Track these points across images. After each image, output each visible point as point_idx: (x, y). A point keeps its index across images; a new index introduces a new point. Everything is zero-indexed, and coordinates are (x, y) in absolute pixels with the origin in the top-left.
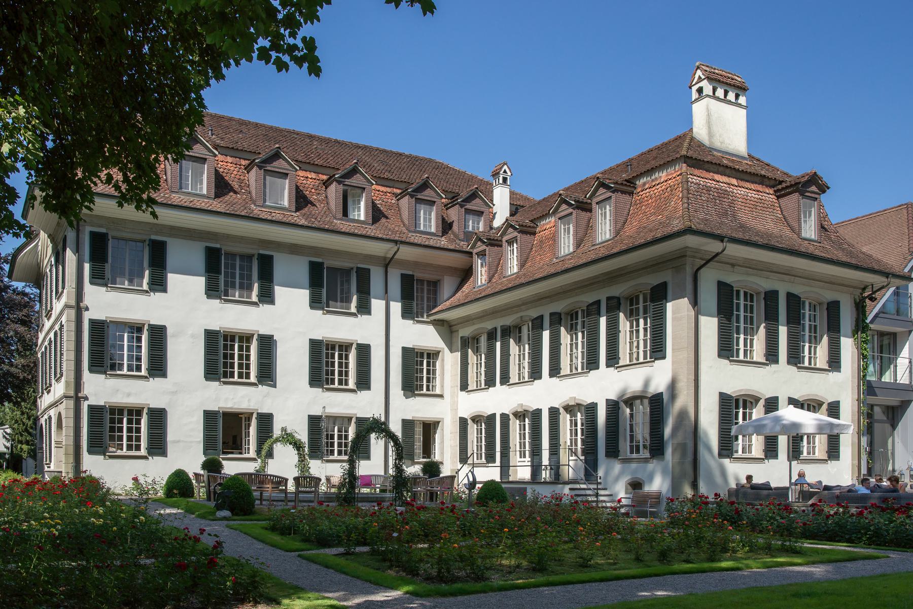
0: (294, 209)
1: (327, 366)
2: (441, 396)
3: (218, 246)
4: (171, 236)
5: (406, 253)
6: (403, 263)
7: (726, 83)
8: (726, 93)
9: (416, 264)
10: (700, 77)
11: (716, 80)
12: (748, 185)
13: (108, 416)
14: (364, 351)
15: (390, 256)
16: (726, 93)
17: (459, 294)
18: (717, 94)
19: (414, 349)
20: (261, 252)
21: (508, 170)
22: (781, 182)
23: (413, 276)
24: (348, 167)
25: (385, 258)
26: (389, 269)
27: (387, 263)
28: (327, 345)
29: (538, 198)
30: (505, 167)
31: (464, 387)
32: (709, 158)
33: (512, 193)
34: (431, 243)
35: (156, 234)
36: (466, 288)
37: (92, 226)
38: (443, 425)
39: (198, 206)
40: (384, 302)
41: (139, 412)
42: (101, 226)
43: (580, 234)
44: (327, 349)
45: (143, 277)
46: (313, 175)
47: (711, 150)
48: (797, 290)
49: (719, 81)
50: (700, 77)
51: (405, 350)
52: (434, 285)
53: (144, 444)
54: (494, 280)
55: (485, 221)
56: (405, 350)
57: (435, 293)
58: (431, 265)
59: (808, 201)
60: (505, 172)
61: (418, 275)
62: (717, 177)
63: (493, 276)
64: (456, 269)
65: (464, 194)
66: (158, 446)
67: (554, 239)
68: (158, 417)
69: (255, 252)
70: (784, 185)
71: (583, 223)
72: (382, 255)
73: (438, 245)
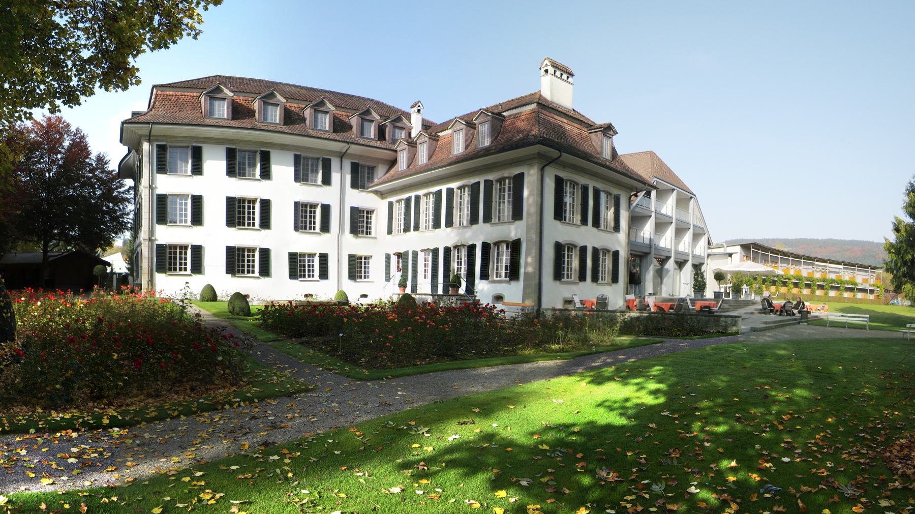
0: (282, 123)
1: (302, 217)
2: (375, 238)
3: (234, 147)
4: (204, 143)
5: (354, 149)
6: (352, 156)
7: (562, 70)
8: (562, 75)
9: (361, 156)
10: (546, 64)
11: (556, 67)
12: (573, 124)
13: (168, 250)
14: (326, 209)
15: (344, 151)
16: (562, 75)
17: (388, 175)
18: (556, 74)
19: (358, 208)
20: (262, 149)
21: (421, 106)
22: (591, 126)
23: (358, 164)
24: (318, 100)
25: (340, 152)
26: (343, 159)
27: (342, 156)
28: (302, 205)
29: (439, 123)
30: (419, 104)
31: (390, 232)
32: (551, 106)
33: (423, 120)
34: (371, 144)
35: (196, 142)
36: (392, 172)
37: (158, 141)
38: (377, 213)
39: (221, 124)
40: (340, 175)
41: (186, 247)
42: (162, 141)
43: (468, 142)
44: (302, 207)
45: (187, 162)
46: (296, 105)
47: (552, 103)
48: (599, 186)
49: (558, 68)
50: (546, 64)
51: (352, 208)
52: (372, 170)
53: (189, 266)
54: (411, 167)
55: (406, 133)
56: (352, 208)
57: (373, 174)
58: (370, 157)
59: (607, 138)
60: (419, 106)
61: (361, 162)
62: (556, 117)
63: (410, 164)
64: (386, 160)
65: (393, 117)
66: (197, 268)
67: (450, 143)
68: (197, 251)
69: (259, 149)
70: (593, 127)
71: (470, 136)
72: (339, 150)
73: (375, 145)
